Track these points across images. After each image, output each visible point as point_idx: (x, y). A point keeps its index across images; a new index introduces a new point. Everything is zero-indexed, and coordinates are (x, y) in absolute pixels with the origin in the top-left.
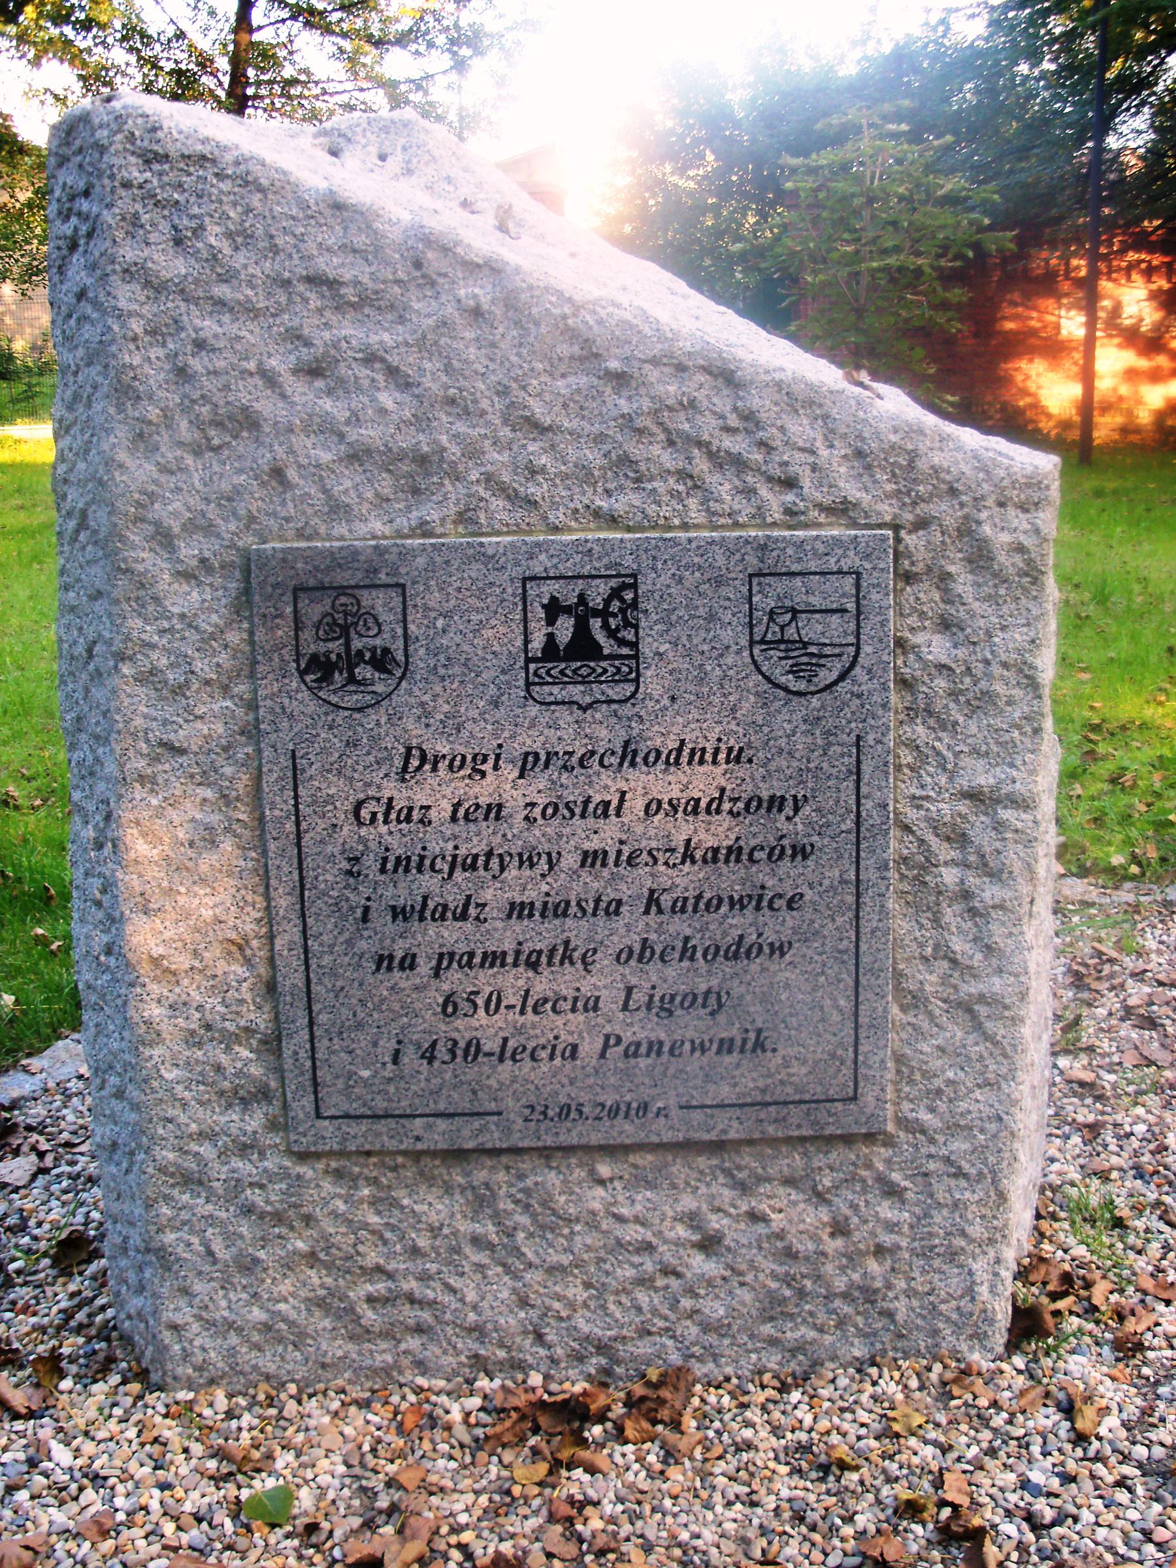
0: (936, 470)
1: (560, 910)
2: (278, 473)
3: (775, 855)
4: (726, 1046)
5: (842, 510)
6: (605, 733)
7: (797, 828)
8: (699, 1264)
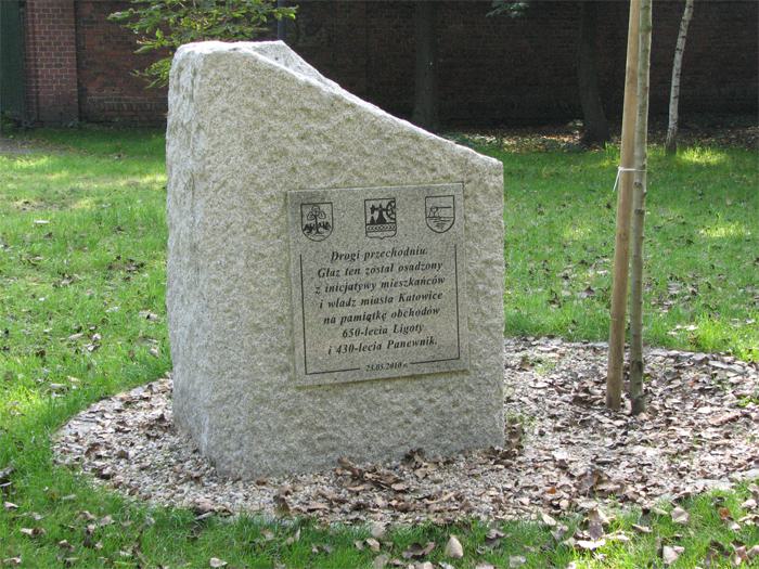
0: (473, 165)
1: (376, 302)
2: (293, 169)
3: (434, 282)
4: (423, 342)
5: (447, 178)
6: (388, 247)
7: (440, 274)
8: (417, 419)
